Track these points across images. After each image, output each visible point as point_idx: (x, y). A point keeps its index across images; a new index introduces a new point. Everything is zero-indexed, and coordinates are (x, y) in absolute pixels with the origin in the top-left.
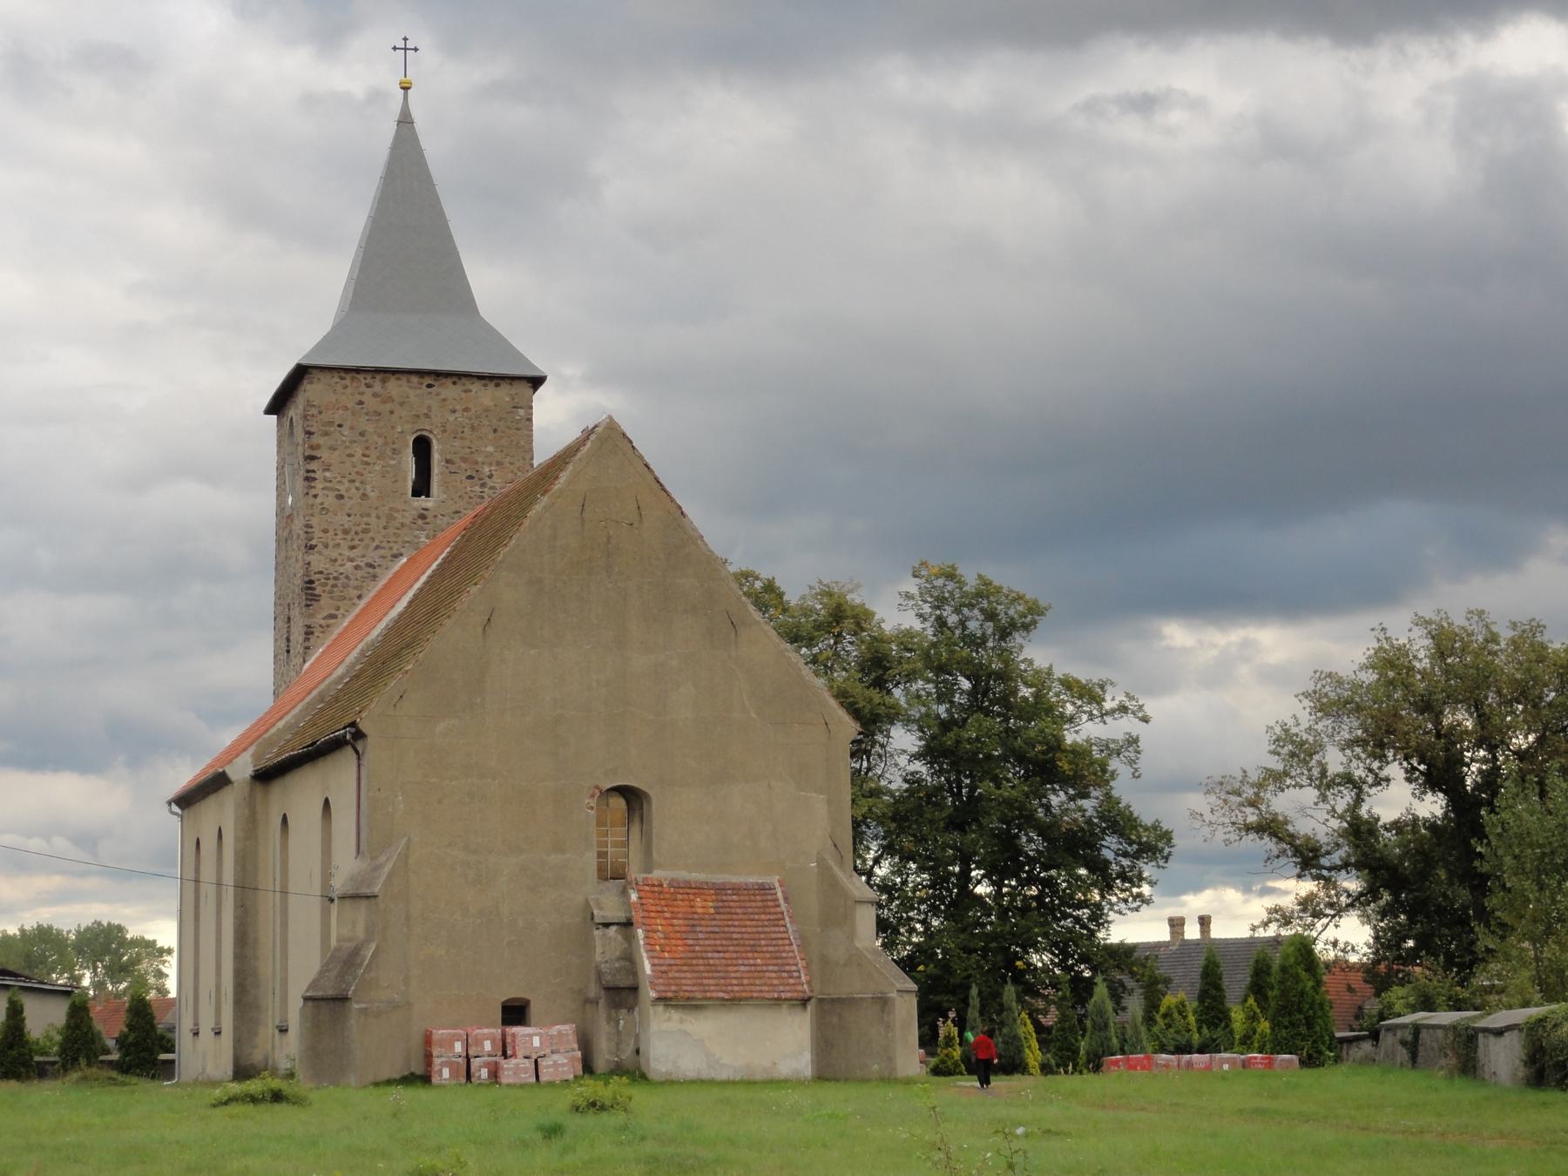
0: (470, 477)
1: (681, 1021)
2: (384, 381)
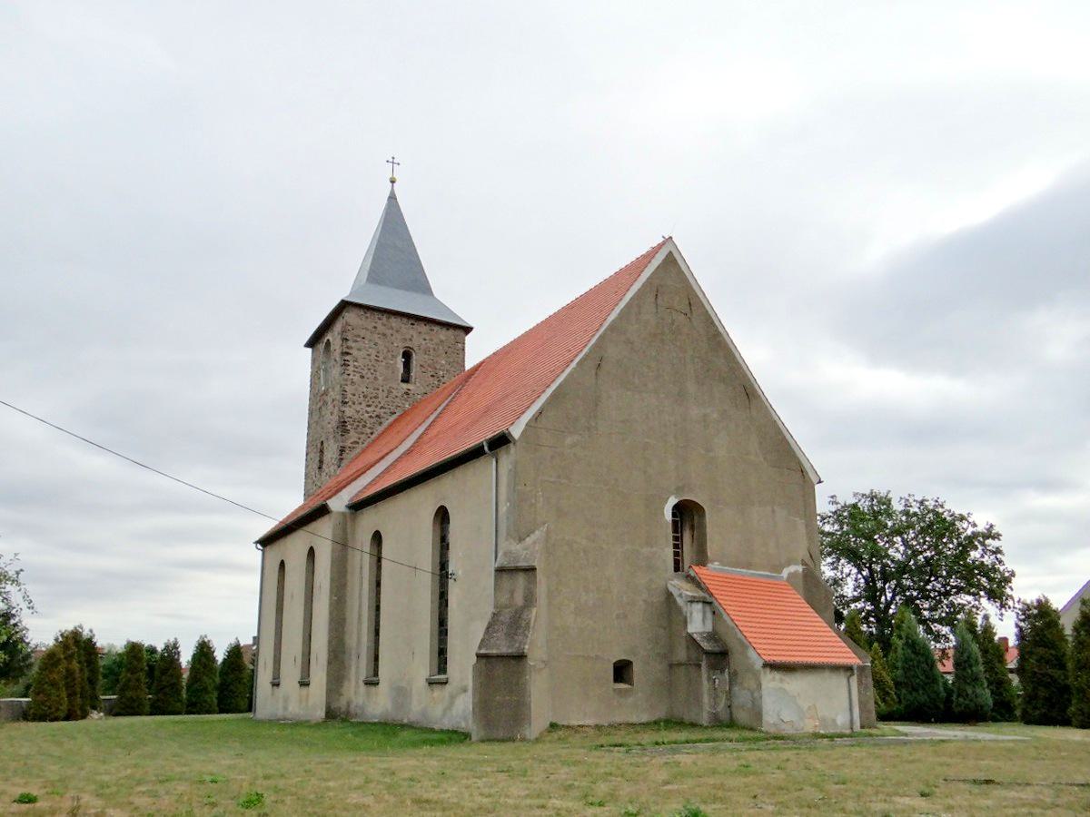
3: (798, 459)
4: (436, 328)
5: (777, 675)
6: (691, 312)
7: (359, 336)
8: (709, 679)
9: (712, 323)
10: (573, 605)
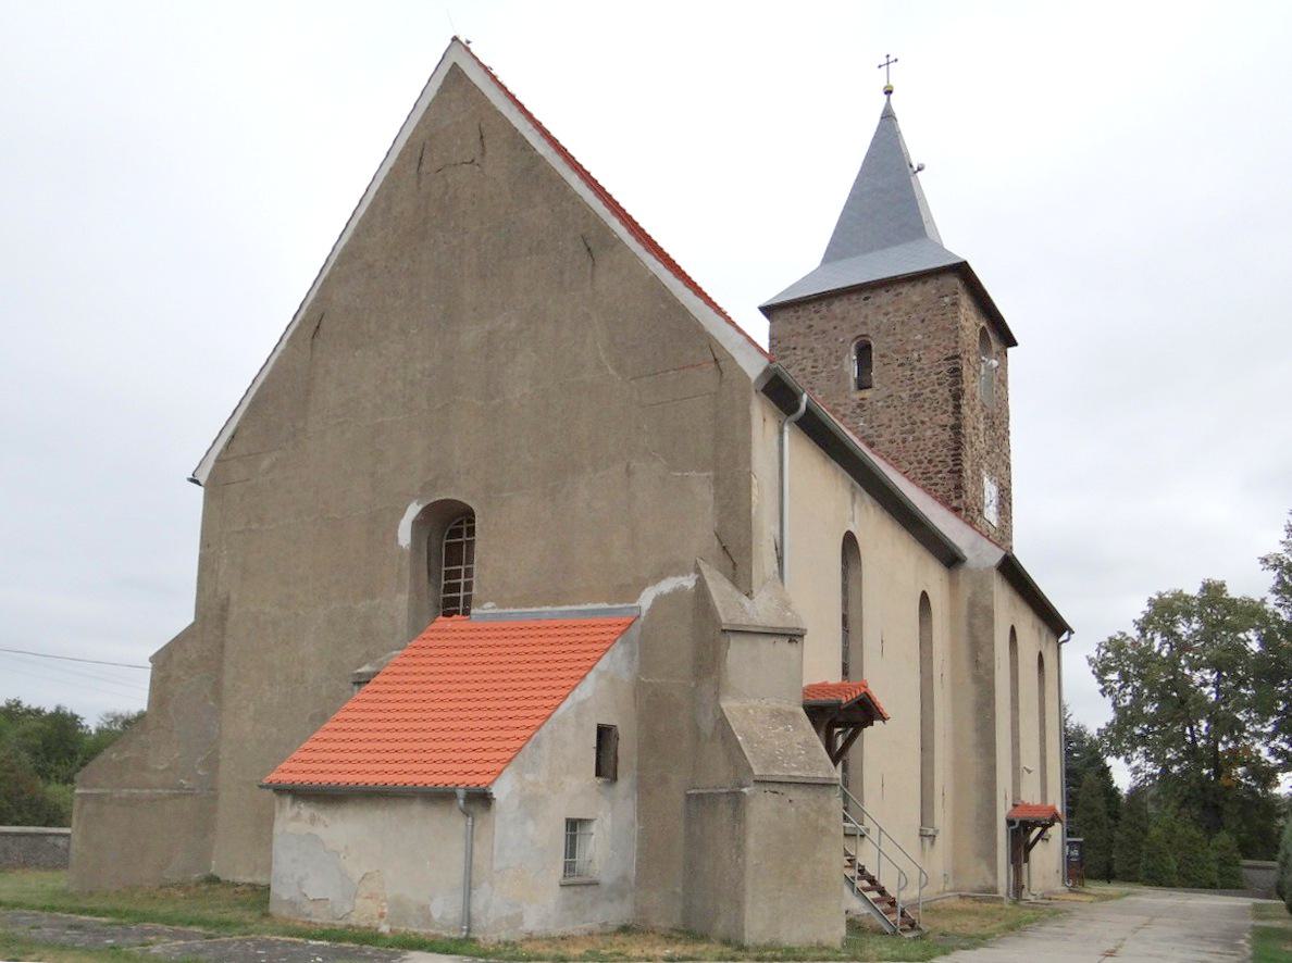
0: (902, 365)
1: (313, 820)
2: (829, 305)
4: (905, 289)
5: (306, 810)
7: (788, 348)
10: (252, 708)
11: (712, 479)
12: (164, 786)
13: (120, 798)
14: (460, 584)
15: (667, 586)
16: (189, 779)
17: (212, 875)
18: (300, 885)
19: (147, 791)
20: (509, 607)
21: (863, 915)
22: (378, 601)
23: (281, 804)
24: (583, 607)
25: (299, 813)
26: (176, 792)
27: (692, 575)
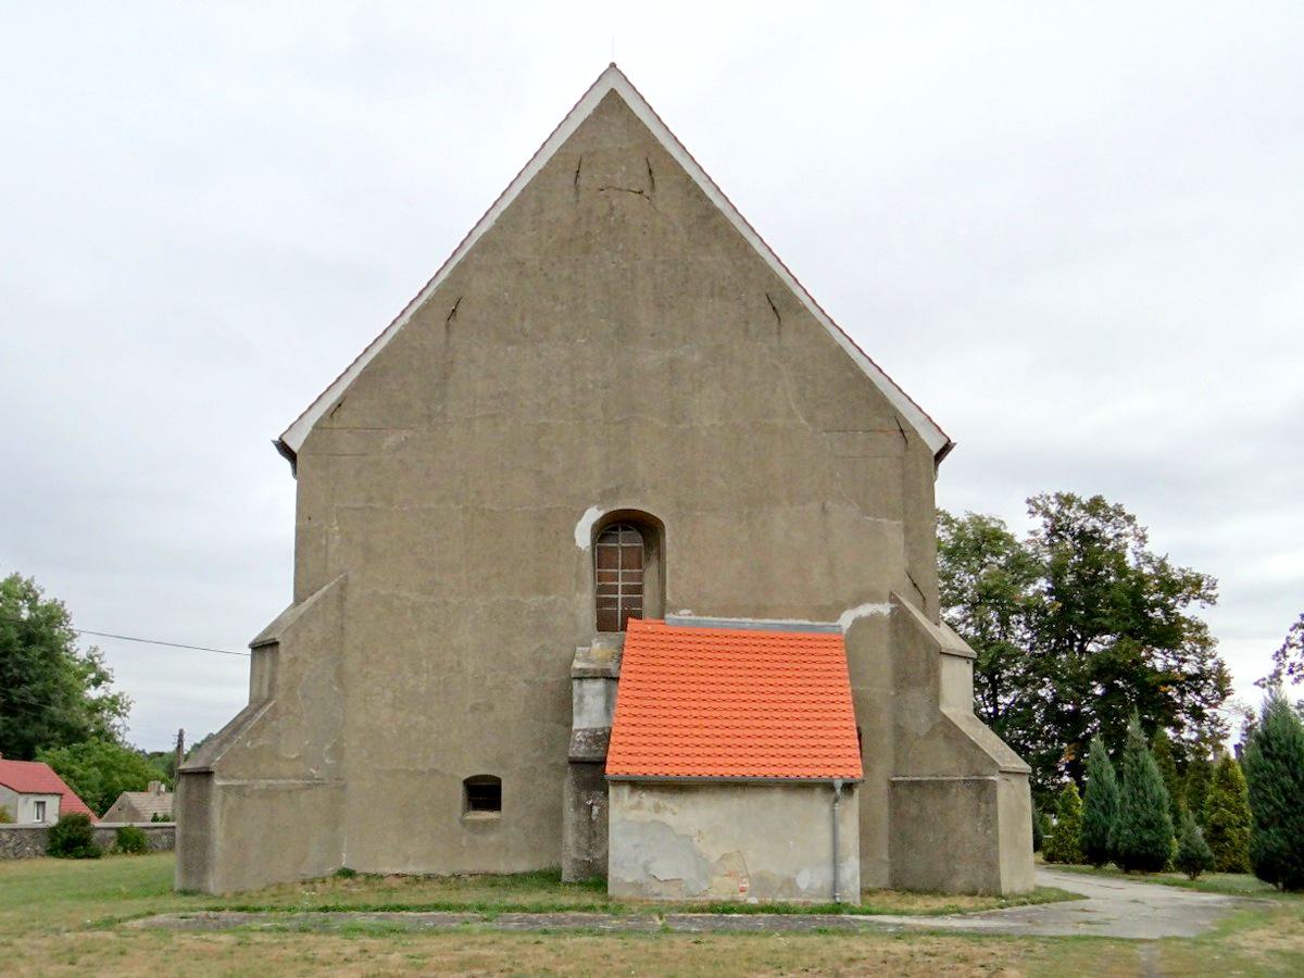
1: (657, 808)
3: (894, 409)
6: (653, 188)
8: (578, 804)
9: (701, 195)
10: (389, 694)
11: (902, 527)
12: (297, 777)
13: (260, 790)
14: (623, 580)
15: (865, 610)
16: (317, 769)
17: (344, 869)
18: (646, 868)
19: (281, 782)
20: (707, 615)
21: (40, 938)
22: (552, 597)
23: (617, 795)
24: (784, 622)
25: (639, 803)
26: (308, 782)
27: (887, 604)
